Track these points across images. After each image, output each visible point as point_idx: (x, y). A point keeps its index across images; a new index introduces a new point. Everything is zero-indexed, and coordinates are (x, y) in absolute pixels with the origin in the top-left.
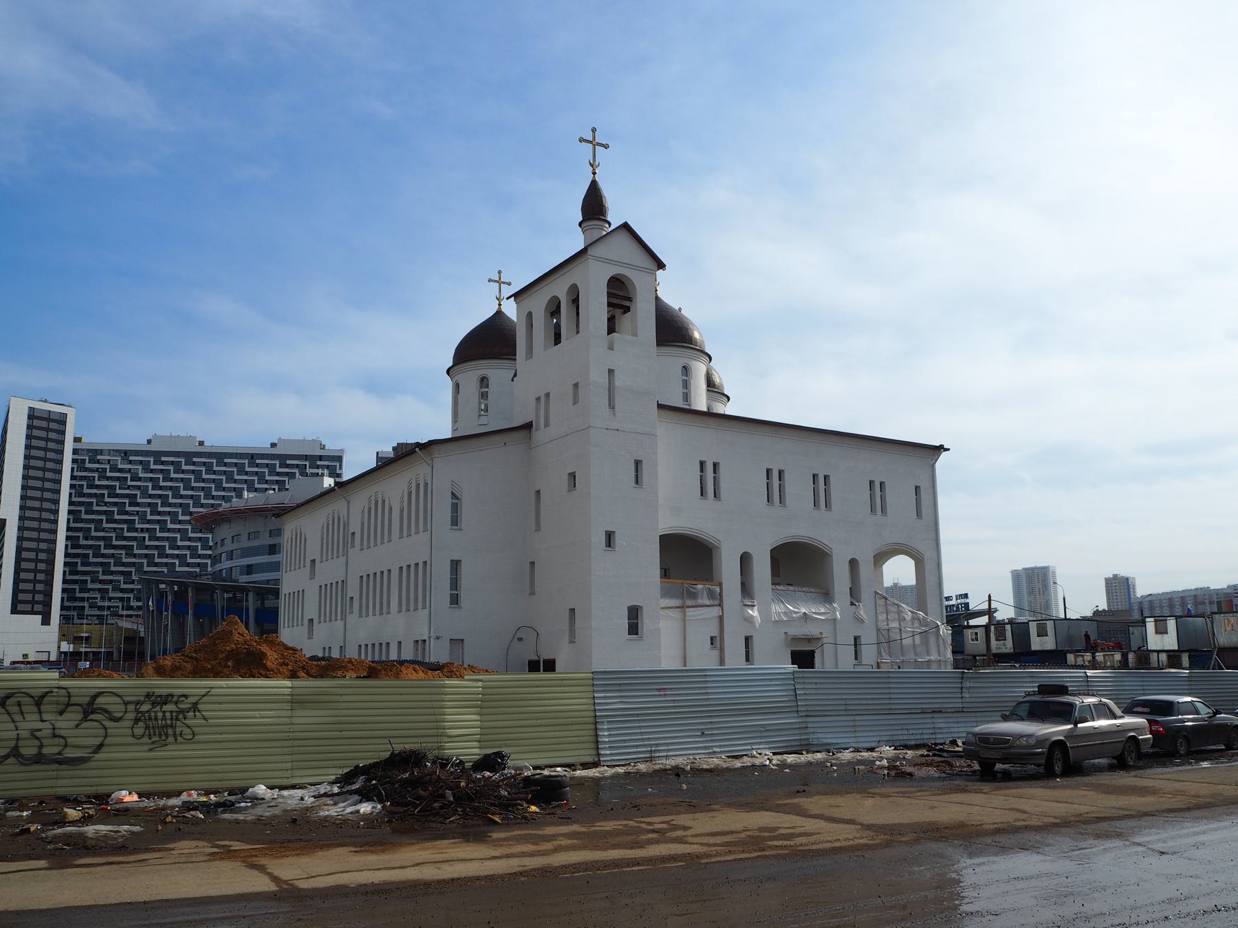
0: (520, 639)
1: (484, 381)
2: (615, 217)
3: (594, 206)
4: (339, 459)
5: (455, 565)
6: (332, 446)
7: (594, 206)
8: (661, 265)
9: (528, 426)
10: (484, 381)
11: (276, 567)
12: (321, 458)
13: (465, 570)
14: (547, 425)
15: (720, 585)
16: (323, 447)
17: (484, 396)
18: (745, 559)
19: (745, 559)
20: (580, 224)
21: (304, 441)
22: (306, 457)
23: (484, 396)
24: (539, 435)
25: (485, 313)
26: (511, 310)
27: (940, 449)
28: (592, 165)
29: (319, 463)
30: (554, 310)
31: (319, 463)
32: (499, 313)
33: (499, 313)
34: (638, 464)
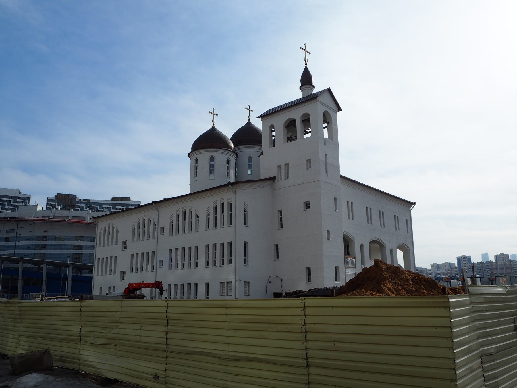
0: (270, 282)
1: (212, 159)
2: (318, 86)
3: (306, 79)
4: (28, 199)
5: (246, 243)
6: (25, 192)
7: (306, 79)
8: (340, 109)
9: (273, 179)
10: (212, 159)
11: (92, 248)
12: (19, 198)
13: (250, 246)
14: (287, 177)
15: (355, 258)
16: (20, 193)
17: (212, 166)
18: (362, 246)
19: (362, 246)
20: (300, 88)
21: (11, 190)
22: (11, 197)
23: (212, 166)
24: (280, 183)
25: (242, 123)
26: (258, 124)
27: (414, 204)
28: (305, 61)
29: (18, 200)
30: (291, 125)
31: (18, 200)
32: (249, 123)
33: (249, 123)
34: (335, 199)
